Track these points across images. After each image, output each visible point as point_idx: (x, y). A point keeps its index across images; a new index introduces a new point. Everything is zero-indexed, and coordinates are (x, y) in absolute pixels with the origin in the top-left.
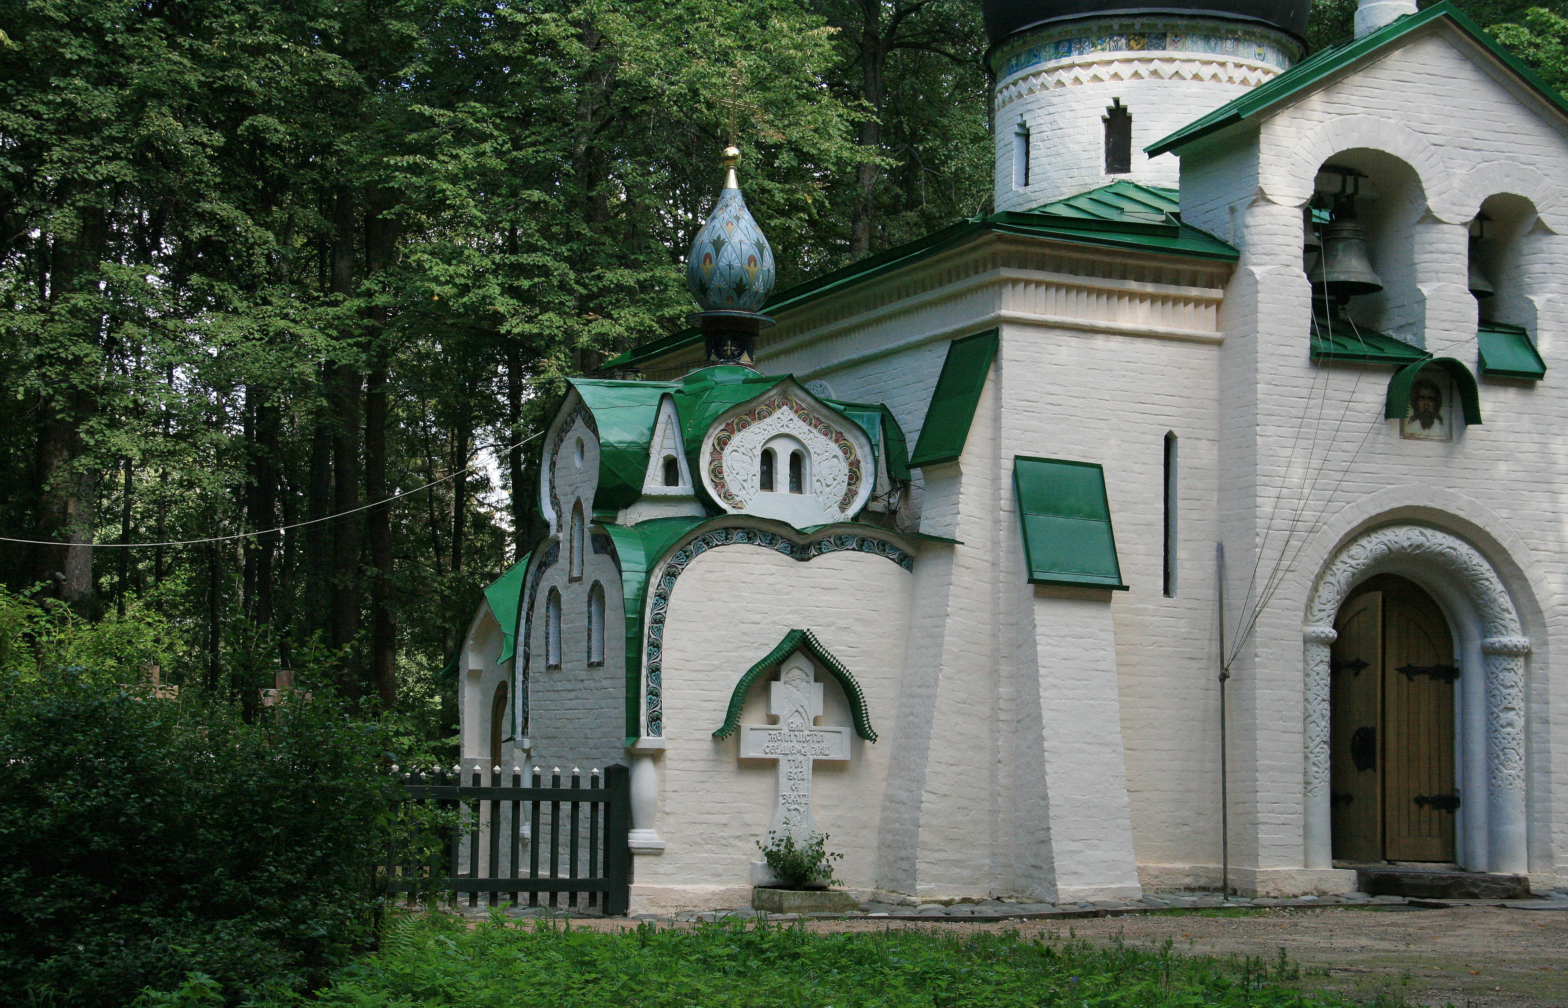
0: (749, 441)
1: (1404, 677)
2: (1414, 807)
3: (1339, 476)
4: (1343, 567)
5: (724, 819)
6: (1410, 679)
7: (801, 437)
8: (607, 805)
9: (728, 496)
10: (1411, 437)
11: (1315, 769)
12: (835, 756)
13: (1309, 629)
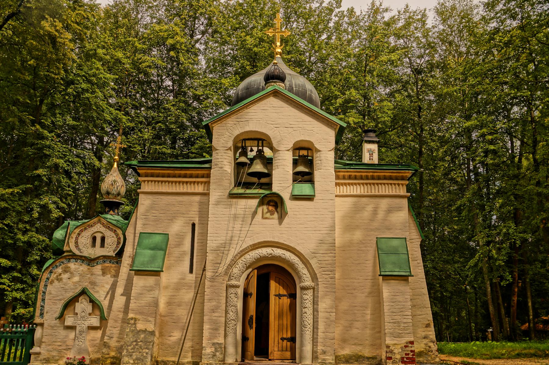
2: (280, 341)
3: (239, 232)
4: (241, 262)
5: (60, 344)
6: (280, 298)
8: (23, 340)
9: (79, 250)
10: (266, 218)
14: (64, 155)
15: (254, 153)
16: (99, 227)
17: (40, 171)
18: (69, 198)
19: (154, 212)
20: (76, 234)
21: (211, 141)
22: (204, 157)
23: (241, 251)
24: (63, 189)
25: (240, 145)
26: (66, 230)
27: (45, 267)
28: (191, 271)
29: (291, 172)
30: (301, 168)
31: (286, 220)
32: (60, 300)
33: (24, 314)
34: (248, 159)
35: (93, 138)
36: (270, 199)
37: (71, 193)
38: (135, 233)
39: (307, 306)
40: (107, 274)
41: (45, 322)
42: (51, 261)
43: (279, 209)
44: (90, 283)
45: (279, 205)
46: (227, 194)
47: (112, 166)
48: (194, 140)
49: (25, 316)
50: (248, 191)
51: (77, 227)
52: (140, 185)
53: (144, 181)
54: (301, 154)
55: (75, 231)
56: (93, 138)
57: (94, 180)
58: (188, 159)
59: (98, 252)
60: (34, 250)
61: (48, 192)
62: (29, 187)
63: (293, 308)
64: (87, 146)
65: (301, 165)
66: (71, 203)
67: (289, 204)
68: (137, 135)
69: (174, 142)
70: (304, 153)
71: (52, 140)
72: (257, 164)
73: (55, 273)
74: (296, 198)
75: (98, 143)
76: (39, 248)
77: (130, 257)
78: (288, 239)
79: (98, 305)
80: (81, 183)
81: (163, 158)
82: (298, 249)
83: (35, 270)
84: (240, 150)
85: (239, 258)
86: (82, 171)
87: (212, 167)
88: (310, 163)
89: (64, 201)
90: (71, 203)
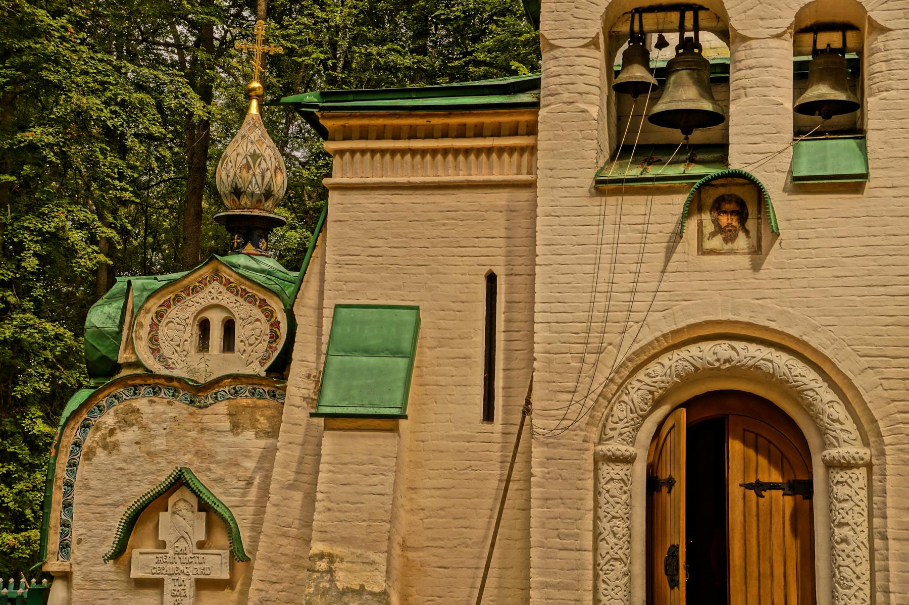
0: (184, 314)
1: (752, 493)
3: (627, 297)
4: (637, 385)
6: (759, 495)
7: (229, 306)
9: (162, 359)
10: (712, 252)
11: (604, 586)
12: (215, 575)
13: (603, 448)
14: (102, 83)
15: (669, 53)
16: (214, 293)
17: (35, 134)
18: (122, 211)
19: (373, 242)
20: (152, 314)
21: (535, 22)
22: (515, 73)
23: (637, 354)
24: (103, 185)
25: (625, 28)
26: (121, 303)
27: (66, 413)
28: (488, 415)
29: (789, 106)
30: (822, 91)
31: (774, 256)
32: (116, 505)
33: (13, 549)
34: (651, 71)
35: (179, 28)
36: (722, 191)
37: (127, 195)
38: (320, 308)
39: (848, 519)
40: (244, 429)
41: (75, 568)
42: (82, 395)
43: (751, 224)
44: (196, 453)
45: (752, 209)
46: (589, 182)
47: (243, 112)
48: (482, 21)
49: (16, 555)
50: (654, 171)
51: (154, 293)
52: (328, 166)
53: (341, 152)
54: (821, 45)
55: (148, 305)
56: (179, 28)
57: (191, 158)
58: (467, 80)
59: (215, 363)
60: (30, 366)
61: (61, 197)
62: (7, 182)
63: (802, 524)
64: (166, 55)
65: (821, 80)
66: (129, 227)
67: (781, 203)
68: (311, 15)
69: (422, 33)
70: (834, 39)
71: (63, 39)
72: (678, 85)
73: (98, 429)
74: (801, 184)
75: (197, 44)
76: (46, 359)
77: (309, 377)
78: (783, 313)
79: (223, 518)
80: (155, 165)
81: (392, 83)
82: (813, 343)
83: (39, 421)
84: (626, 46)
85: (629, 377)
86: (157, 130)
87: (542, 103)
88: (851, 73)
89: (111, 219)
90: (129, 227)
